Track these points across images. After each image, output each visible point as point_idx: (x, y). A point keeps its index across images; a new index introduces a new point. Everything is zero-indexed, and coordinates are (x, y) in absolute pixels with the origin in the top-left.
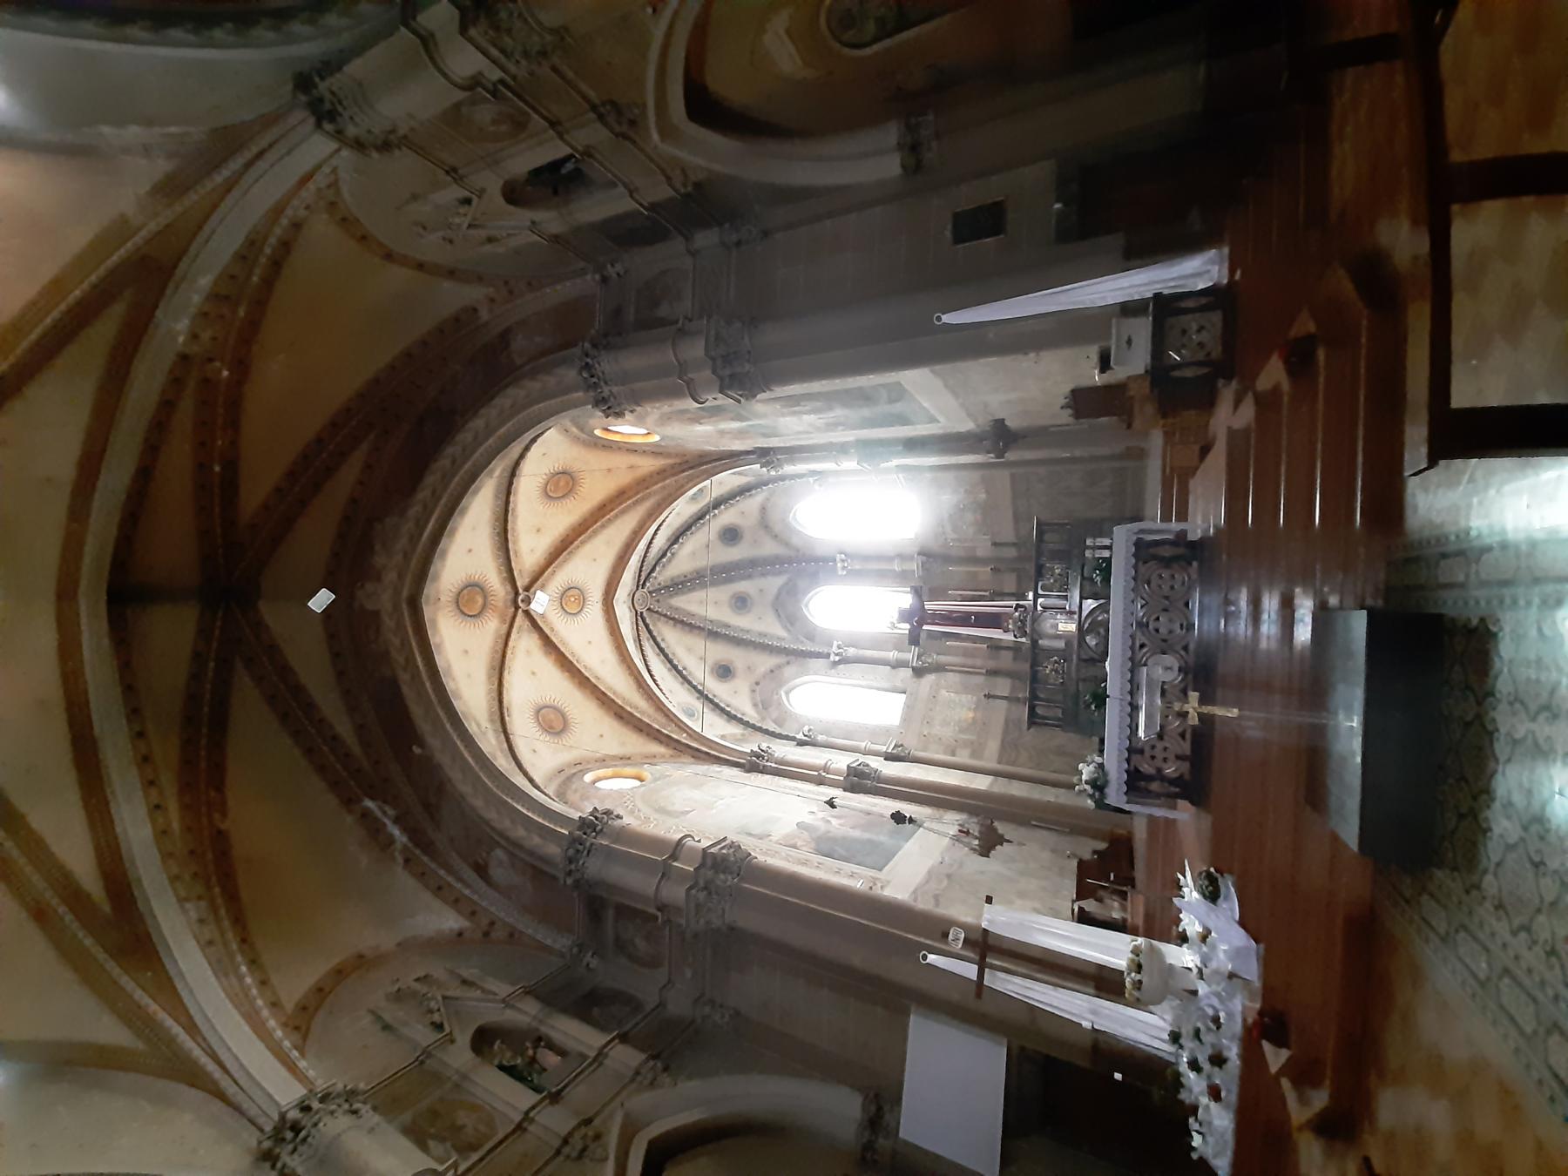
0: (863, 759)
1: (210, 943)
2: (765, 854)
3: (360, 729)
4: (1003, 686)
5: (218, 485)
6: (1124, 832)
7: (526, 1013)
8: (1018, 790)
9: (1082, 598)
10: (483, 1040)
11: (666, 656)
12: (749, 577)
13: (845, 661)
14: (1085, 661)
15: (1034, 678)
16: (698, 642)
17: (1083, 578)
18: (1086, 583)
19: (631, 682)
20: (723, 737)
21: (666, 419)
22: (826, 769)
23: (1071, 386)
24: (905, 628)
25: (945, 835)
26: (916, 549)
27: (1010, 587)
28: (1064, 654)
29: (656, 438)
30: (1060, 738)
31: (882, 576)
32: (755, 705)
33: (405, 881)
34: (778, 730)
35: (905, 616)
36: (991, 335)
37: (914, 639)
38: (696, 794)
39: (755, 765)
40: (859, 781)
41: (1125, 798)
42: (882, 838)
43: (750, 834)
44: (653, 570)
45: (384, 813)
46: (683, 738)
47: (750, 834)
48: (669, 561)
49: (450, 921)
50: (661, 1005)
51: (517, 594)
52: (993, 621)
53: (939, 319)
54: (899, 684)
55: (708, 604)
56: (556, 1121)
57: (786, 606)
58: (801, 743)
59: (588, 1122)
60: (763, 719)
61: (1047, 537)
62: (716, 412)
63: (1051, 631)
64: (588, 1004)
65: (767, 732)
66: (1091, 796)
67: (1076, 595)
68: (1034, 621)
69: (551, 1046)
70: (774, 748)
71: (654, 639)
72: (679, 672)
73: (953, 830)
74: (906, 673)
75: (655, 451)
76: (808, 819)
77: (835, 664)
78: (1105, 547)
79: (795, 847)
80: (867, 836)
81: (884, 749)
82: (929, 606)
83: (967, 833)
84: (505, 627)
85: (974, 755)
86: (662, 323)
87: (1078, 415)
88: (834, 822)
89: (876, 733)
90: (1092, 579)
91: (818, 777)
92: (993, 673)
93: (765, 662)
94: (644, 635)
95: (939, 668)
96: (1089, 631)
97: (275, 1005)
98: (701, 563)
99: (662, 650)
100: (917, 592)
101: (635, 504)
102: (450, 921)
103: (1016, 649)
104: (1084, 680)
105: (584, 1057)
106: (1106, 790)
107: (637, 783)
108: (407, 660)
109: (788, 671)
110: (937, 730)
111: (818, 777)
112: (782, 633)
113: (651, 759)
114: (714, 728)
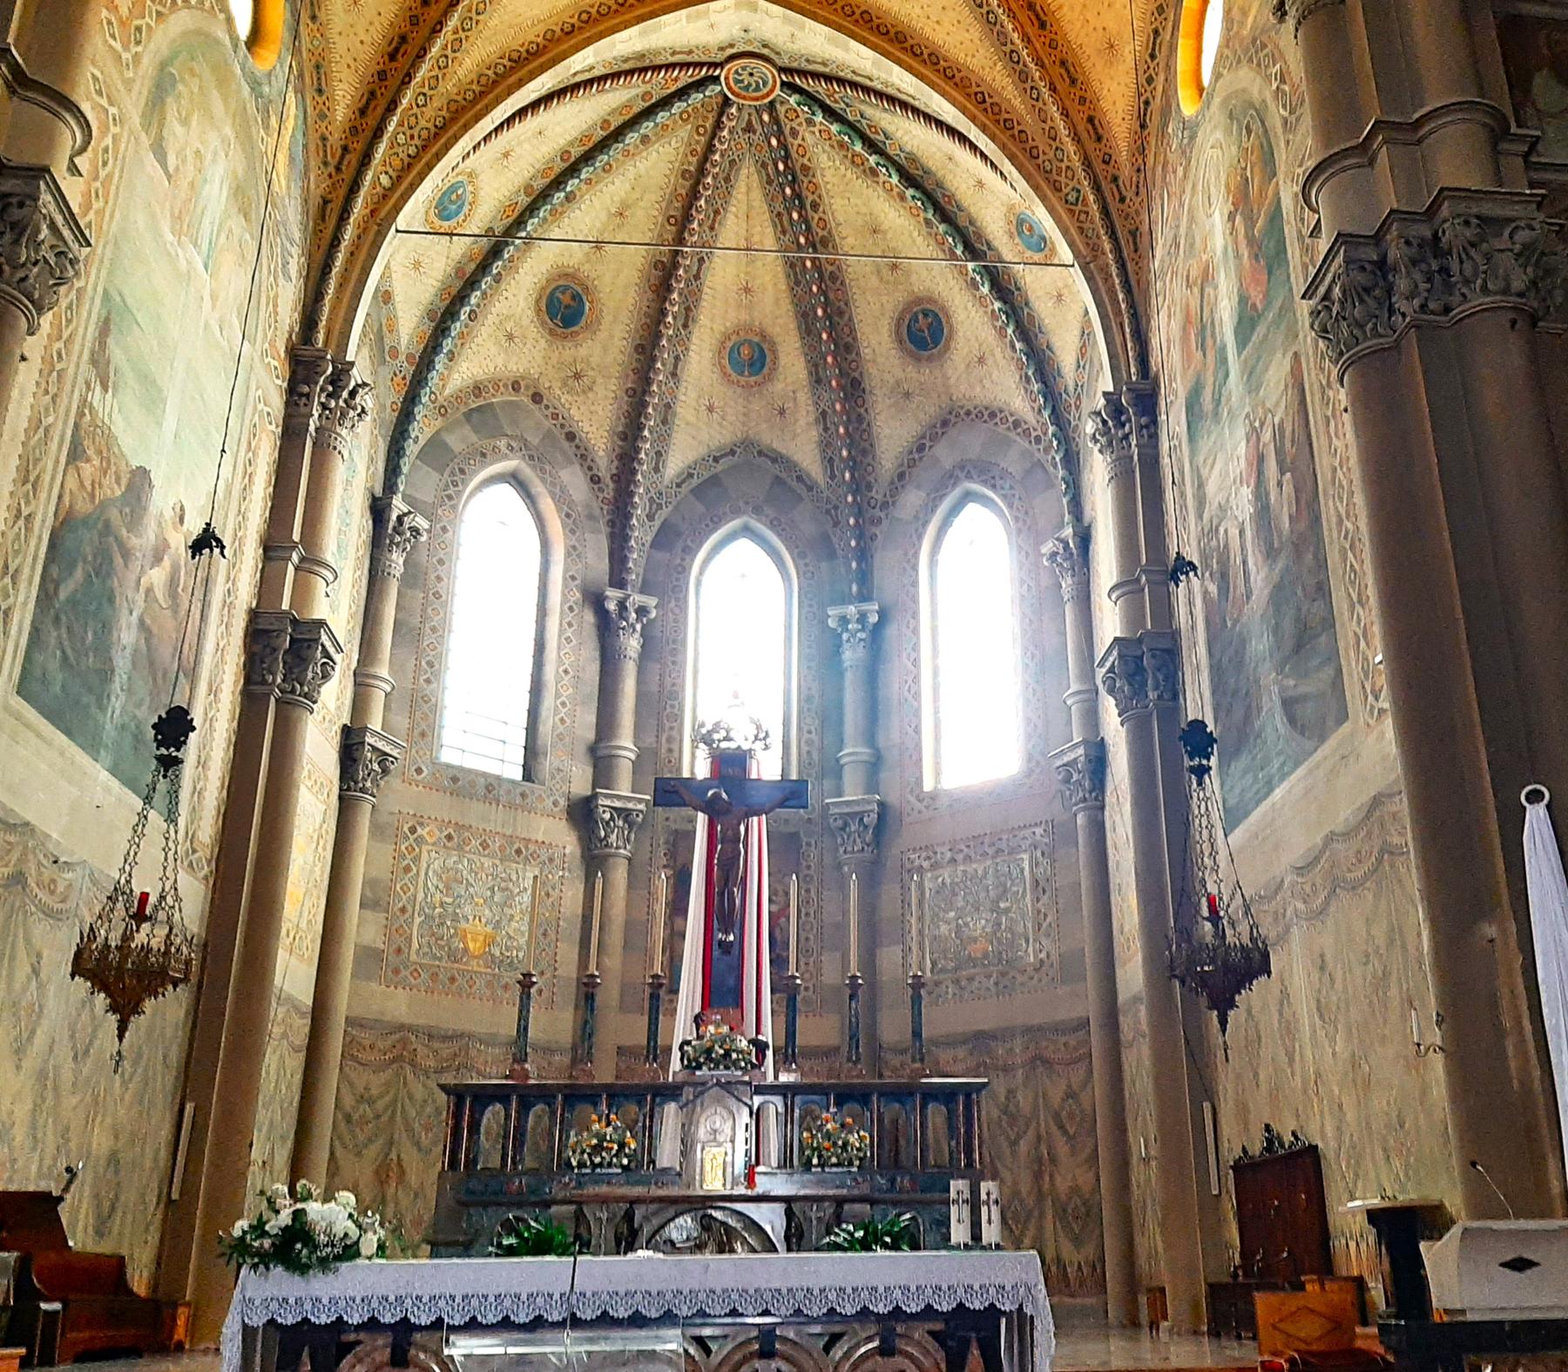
0: (345, 662)
2: (50, 365)
4: (553, 1023)
6: (180, 1333)
8: (278, 1068)
9: (787, 1200)
11: (603, 145)
12: (817, 380)
13: (606, 628)
14: (629, 1216)
15: (578, 1096)
16: (646, 222)
17: (839, 1202)
18: (829, 1208)
19: (533, 35)
20: (385, 297)
21: (1247, 120)
22: (311, 563)
23: (1327, 1146)
24: (699, 766)
25: (130, 860)
26: (893, 798)
27: (811, 1031)
28: (641, 1164)
29: (1188, 106)
30: (424, 1170)
31: (820, 715)
32: (477, 389)
34: (412, 449)
35: (731, 765)
36: (1491, 931)
37: (671, 792)
38: (216, 195)
39: (311, 372)
40: (281, 652)
41: (258, 1321)
42: (117, 703)
43: (105, 329)
44: (831, 114)
46: (376, 176)
47: (105, 329)
48: (855, 161)
52: (721, 991)
53: (1534, 797)
54: (547, 764)
55: (743, 272)
57: (749, 482)
58: (378, 509)
60: (442, 411)
61: (936, 1114)
62: (1266, 251)
63: (702, 1133)
65: (405, 416)
66: (259, 1229)
67: (781, 1185)
68: (727, 1086)
70: (365, 427)
71: (648, 113)
72: (558, 183)
73: (145, 882)
74: (580, 781)
75: (1151, 110)
76: (161, 501)
77: (595, 601)
78: (976, 1236)
79: (76, 453)
80: (122, 663)
81: (375, 723)
82: (757, 830)
83: (140, 917)
85: (369, 958)
86: (1519, 84)
87: (1244, 1168)
88: (157, 577)
89: (421, 708)
90: (838, 1219)
91: (287, 539)
92: (587, 992)
93: (596, 419)
94: (660, 85)
95: (594, 860)
96: (707, 1224)
98: (849, 240)
99: (617, 134)
100: (791, 794)
101: (1012, 57)
103: (655, 1051)
104: (579, 1217)
106: (278, 1271)
107: (243, 28)
109: (574, 480)
110: (432, 862)
111: (287, 539)
112: (674, 465)
113: (314, 78)
114: (409, 267)
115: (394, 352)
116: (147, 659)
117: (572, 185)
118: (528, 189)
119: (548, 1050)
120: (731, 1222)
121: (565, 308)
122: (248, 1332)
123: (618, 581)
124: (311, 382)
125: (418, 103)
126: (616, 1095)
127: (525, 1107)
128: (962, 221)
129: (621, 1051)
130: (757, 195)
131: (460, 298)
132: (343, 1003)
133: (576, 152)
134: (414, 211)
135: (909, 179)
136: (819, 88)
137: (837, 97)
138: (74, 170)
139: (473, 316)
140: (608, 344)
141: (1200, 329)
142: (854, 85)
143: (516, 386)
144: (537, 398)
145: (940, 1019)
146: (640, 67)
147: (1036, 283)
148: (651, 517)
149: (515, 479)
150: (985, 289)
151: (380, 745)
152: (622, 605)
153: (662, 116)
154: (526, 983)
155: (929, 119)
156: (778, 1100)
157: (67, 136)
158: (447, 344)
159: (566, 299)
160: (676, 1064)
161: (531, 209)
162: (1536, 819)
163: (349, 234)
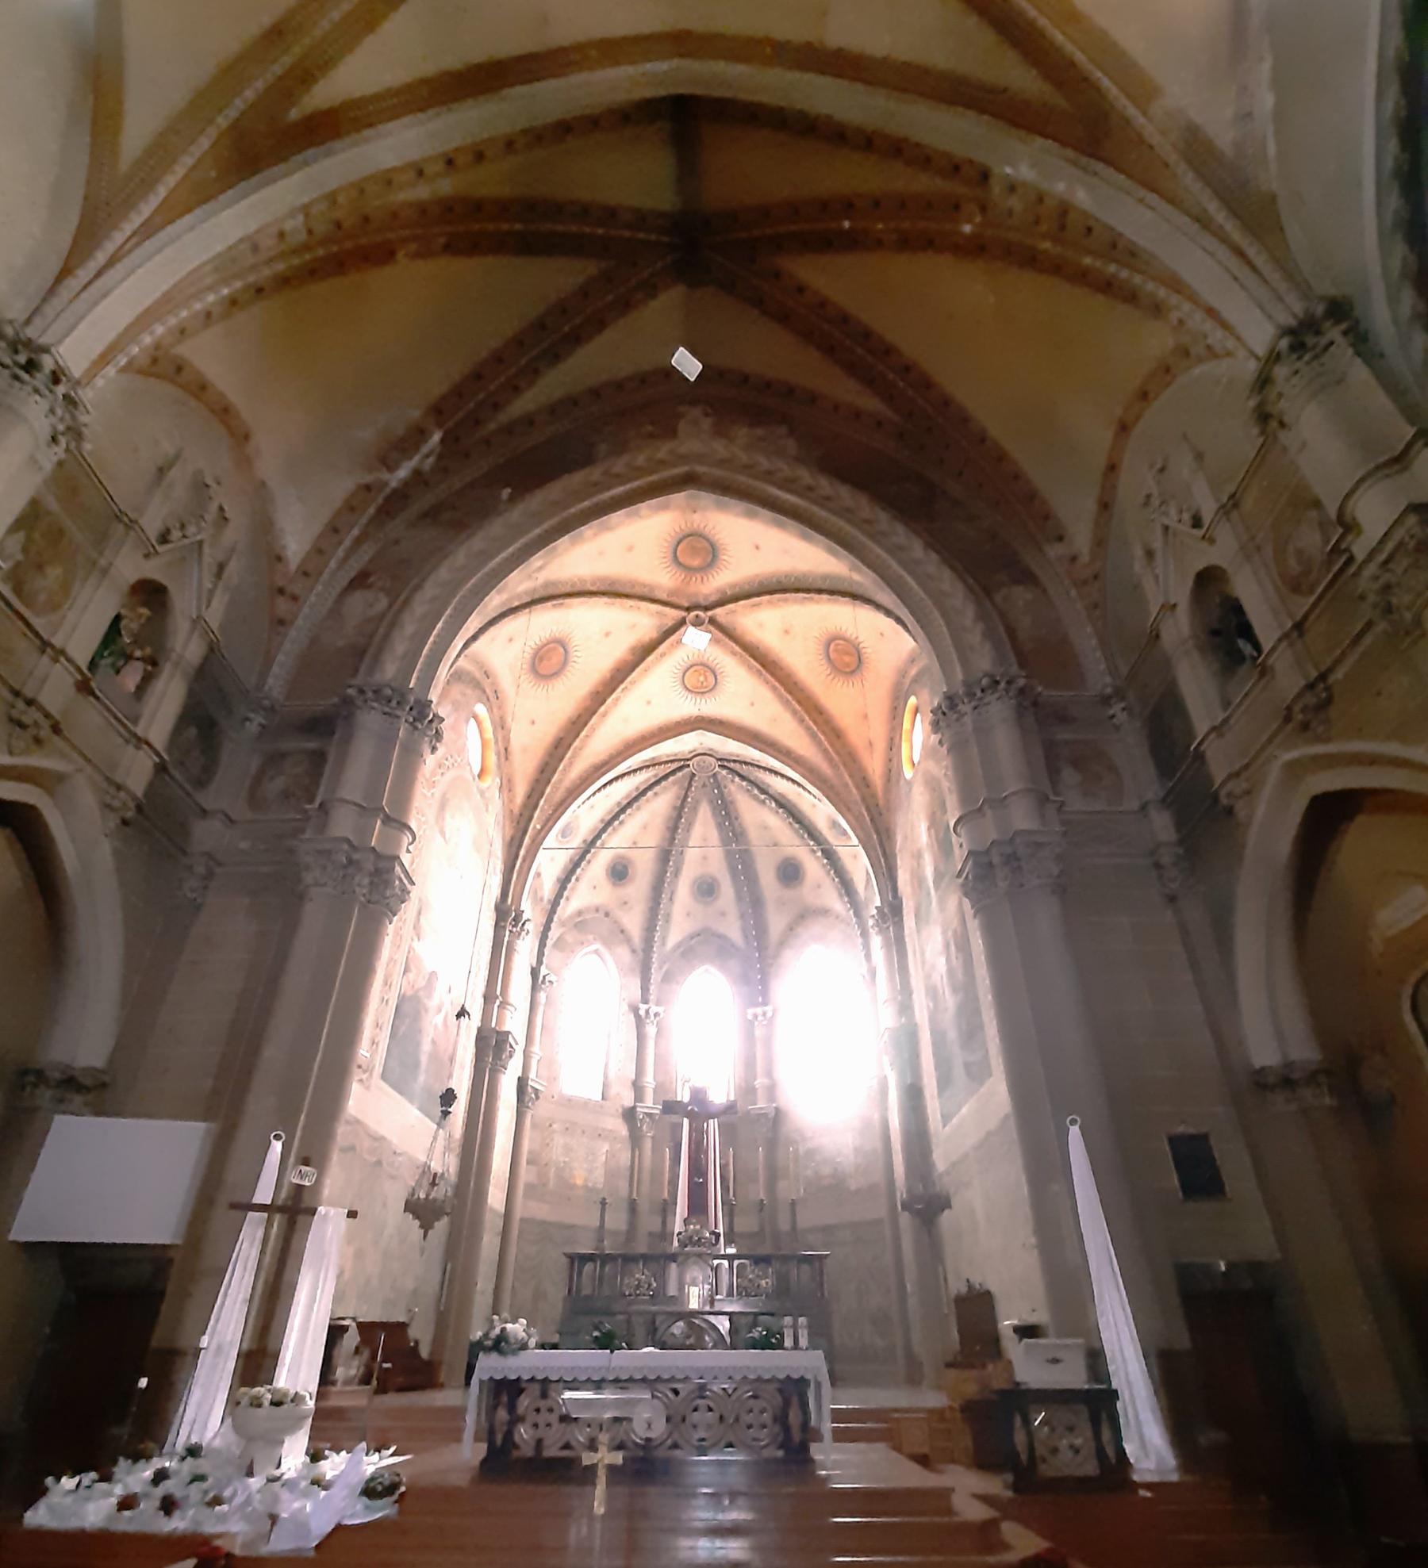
0: (519, 1050)
1: (255, 248)
3: (529, 421)
4: (617, 1221)
5: (827, 228)
7: (186, 647)
8: (489, 1244)
10: (150, 594)
11: (636, 799)
13: (640, 1023)
15: (629, 1259)
16: (653, 838)
17: (756, 1315)
18: (750, 1319)
20: (538, 875)
21: (932, 785)
23: (994, 1289)
24: (684, 1096)
25: (429, 1157)
29: (908, 773)
32: (580, 913)
33: (341, 487)
34: (549, 943)
39: (506, 916)
40: (491, 1047)
41: (486, 1378)
42: (422, 1078)
44: (743, 778)
45: (427, 456)
46: (535, 824)
48: (755, 798)
49: (295, 545)
50: (204, 813)
51: (706, 609)
53: (1073, 1122)
56: (55, 689)
58: (534, 972)
59: (56, 729)
63: (688, 1278)
64: (202, 722)
66: (486, 1336)
68: (700, 1255)
69: (147, 679)
72: (616, 817)
73: (436, 1166)
74: (628, 1100)
77: (635, 1010)
80: (424, 1059)
81: (532, 1075)
82: (713, 1125)
84: (664, 596)
85: (529, 1187)
86: (1053, 772)
88: (438, 1020)
90: (755, 1325)
92: (633, 1207)
93: (633, 921)
95: (635, 1139)
96: (691, 1325)
97: (182, 332)
98: (754, 835)
99: (644, 793)
100: (730, 1108)
102: (295, 545)
103: (665, 1235)
104: (629, 1322)
105: (135, 721)
107: (477, 770)
108: (618, 476)
109: (624, 952)
110: (559, 1141)
113: (507, 786)
114: (549, 863)
115: (542, 899)
116: (434, 1056)
117: (622, 817)
118: (602, 821)
119: (615, 1233)
120: (703, 1325)
121: (619, 873)
122: (481, 1382)
123: (645, 1001)
124: (505, 920)
125: (554, 791)
126: (646, 1258)
127: (602, 1266)
128: (806, 823)
129: (650, 1234)
130: (709, 814)
131: (572, 871)
132: (518, 1213)
133: (625, 802)
134: (551, 840)
135: (780, 805)
136: (737, 766)
137: (744, 770)
138: (408, 851)
139: (577, 880)
140: (639, 888)
141: (918, 880)
142: (752, 765)
143: (597, 910)
144: (607, 915)
145: (805, 1220)
146: (654, 764)
147: (844, 853)
148: (661, 968)
149: (596, 952)
150: (819, 854)
151: (537, 1086)
152: (647, 1012)
153: (663, 783)
154: (603, 1203)
155: (789, 779)
156: (726, 1263)
157: (406, 838)
158: (566, 894)
159: (619, 868)
160: (676, 1243)
161: (604, 830)
162: (1075, 1132)
163: (522, 853)
